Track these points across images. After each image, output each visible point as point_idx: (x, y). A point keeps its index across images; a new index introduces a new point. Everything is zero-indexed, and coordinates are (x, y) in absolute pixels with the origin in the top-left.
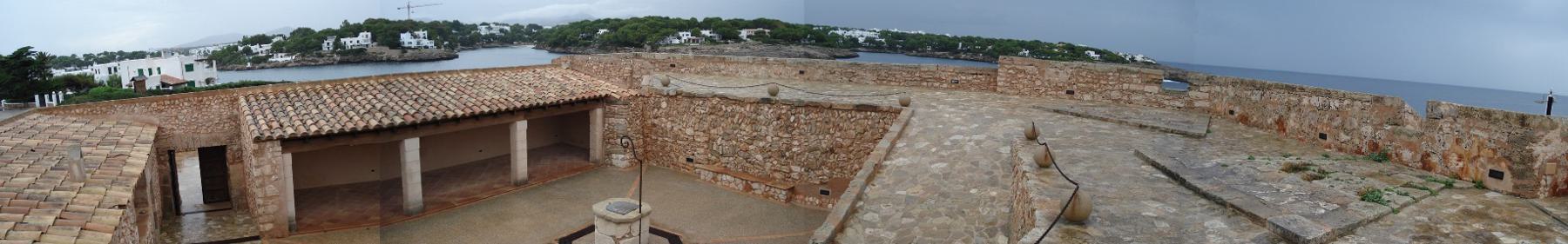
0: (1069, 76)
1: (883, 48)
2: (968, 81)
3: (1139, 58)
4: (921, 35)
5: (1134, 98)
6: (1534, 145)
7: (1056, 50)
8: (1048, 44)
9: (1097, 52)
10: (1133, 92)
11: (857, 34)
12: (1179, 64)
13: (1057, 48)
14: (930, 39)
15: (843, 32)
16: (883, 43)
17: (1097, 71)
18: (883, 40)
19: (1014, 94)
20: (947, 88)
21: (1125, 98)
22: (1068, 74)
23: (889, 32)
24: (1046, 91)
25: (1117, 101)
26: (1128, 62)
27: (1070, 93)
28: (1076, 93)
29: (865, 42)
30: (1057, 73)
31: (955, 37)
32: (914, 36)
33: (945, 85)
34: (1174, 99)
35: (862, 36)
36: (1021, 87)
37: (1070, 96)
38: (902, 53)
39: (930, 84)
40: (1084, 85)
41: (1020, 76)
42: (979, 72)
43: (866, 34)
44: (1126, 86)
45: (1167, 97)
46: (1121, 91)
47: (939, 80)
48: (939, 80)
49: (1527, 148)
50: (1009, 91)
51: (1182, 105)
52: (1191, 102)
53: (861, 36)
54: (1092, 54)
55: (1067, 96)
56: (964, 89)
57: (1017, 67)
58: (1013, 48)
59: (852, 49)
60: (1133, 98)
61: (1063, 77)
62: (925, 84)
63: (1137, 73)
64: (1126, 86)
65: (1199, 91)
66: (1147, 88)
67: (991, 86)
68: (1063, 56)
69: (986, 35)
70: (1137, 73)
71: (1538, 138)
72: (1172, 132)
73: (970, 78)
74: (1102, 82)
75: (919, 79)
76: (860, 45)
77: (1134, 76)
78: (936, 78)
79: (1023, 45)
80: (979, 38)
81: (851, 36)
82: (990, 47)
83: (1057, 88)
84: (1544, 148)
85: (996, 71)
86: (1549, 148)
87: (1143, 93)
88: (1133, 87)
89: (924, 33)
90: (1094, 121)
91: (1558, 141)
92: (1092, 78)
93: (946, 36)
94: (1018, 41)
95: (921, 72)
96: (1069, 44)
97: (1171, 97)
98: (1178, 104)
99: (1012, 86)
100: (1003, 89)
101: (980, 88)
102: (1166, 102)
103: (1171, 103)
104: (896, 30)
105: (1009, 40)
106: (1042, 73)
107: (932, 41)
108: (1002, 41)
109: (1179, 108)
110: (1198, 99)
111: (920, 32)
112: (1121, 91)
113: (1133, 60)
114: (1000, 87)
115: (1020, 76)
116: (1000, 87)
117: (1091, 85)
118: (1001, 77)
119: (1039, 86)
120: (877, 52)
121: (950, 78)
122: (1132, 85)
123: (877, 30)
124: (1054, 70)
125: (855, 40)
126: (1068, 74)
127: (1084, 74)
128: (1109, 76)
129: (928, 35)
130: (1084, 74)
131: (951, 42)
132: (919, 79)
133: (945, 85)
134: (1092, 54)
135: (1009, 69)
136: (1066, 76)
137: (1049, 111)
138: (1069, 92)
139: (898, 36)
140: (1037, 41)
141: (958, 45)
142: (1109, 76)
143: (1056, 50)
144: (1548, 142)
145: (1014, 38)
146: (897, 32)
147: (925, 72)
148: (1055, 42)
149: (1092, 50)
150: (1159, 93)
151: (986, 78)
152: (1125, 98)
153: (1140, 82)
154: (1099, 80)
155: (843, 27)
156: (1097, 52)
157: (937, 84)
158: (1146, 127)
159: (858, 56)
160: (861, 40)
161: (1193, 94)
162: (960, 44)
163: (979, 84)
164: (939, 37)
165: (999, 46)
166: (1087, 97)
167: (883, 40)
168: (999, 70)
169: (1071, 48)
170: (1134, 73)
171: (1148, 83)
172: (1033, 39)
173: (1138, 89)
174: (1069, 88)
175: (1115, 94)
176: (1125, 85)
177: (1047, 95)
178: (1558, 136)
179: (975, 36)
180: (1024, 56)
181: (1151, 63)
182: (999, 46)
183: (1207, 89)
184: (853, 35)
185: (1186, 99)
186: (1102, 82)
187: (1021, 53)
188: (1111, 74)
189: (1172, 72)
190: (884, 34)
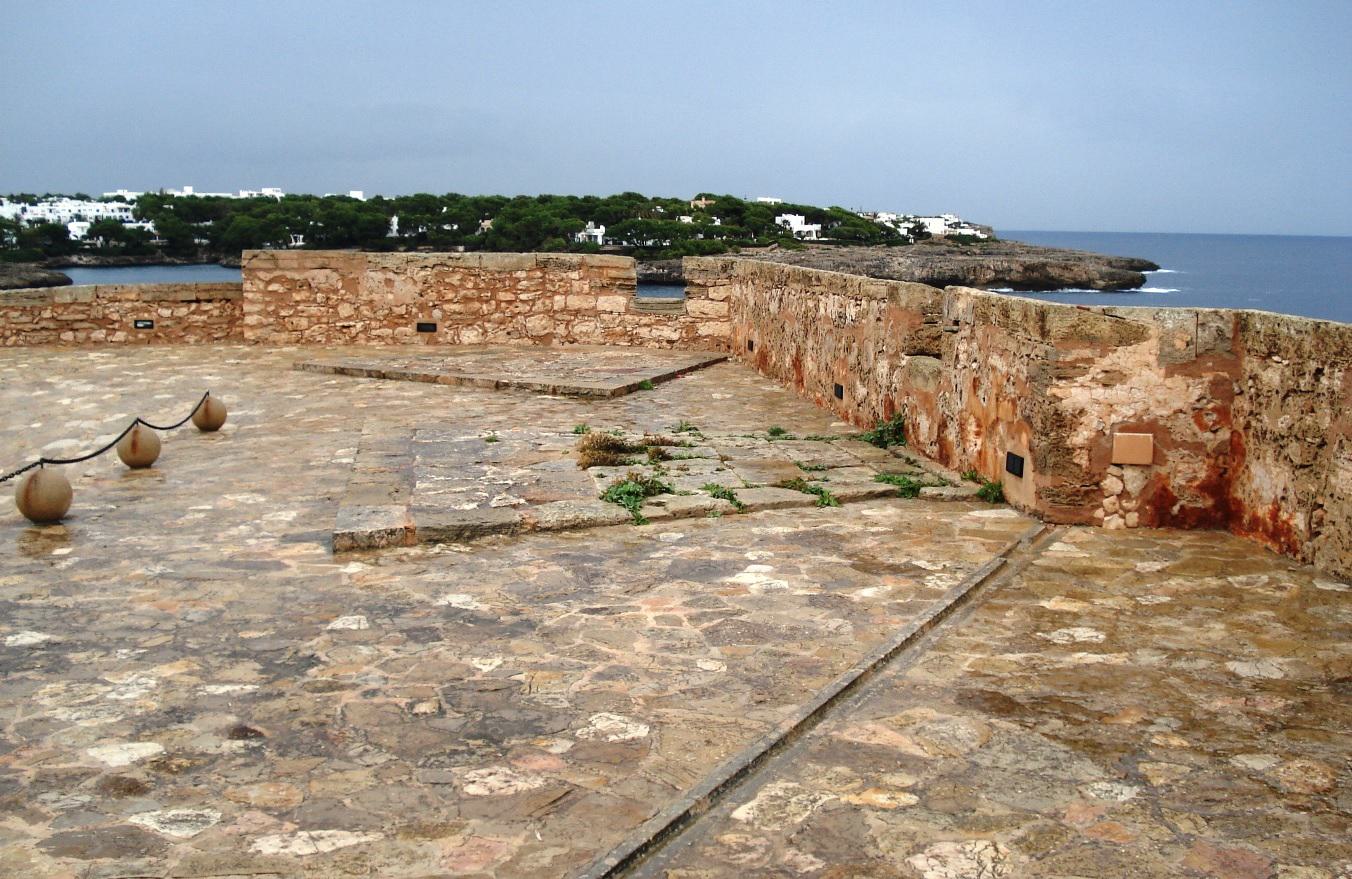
0: (420, 286)
1: (152, 250)
2: (179, 320)
3: (936, 227)
4: (272, 200)
5: (579, 328)
6: (1062, 383)
7: (687, 220)
8: (664, 203)
9: (812, 215)
10: (577, 312)
11: (61, 211)
12: (1024, 234)
13: (689, 213)
14: (299, 211)
15: (16, 208)
16: (149, 235)
17: (485, 270)
18: (149, 226)
19: (288, 343)
20: (125, 343)
21: (561, 330)
22: (415, 282)
23: (164, 198)
24: (366, 329)
25: (544, 340)
26: (904, 241)
27: (426, 328)
28: (442, 328)
29: (92, 233)
30: (389, 282)
31: (379, 199)
32: (247, 206)
33: (120, 336)
34: (658, 322)
35: (79, 218)
36: (304, 322)
37: (427, 335)
38: (214, 261)
39: (81, 335)
40: (456, 307)
41: (297, 297)
42: (203, 296)
43: (93, 210)
44: (559, 301)
45: (645, 320)
46: (550, 313)
47: (103, 322)
48: (103, 322)
49: (1049, 392)
50: (275, 336)
51: (675, 336)
52: (691, 327)
53: (74, 216)
54: (797, 223)
55: (418, 338)
56: (170, 342)
57: (290, 275)
58: (557, 221)
59: (50, 260)
60: (577, 330)
61: (405, 290)
62: (68, 336)
63: (580, 266)
64: (559, 301)
65: (707, 298)
66: (605, 302)
67: (230, 329)
68: (709, 235)
69: (474, 188)
70: (580, 266)
71: (1073, 365)
72: (554, 392)
73: (183, 311)
74: (502, 296)
75: (52, 325)
76: (76, 247)
77: (574, 275)
78: (94, 320)
79: (587, 209)
80: (453, 199)
81: (42, 221)
82: (487, 224)
83: (394, 320)
84: (1099, 392)
85: (239, 288)
86: (1118, 392)
87: (596, 313)
88: (574, 302)
89: (279, 195)
90: (399, 384)
91: (1155, 375)
92: (476, 287)
93: (350, 200)
94: (572, 198)
95: (55, 306)
96: (728, 199)
97: (653, 319)
98: (668, 333)
99: (281, 325)
100: (259, 332)
101: (208, 334)
102: (644, 332)
103: (655, 333)
104: (188, 191)
105: (544, 200)
106: (352, 285)
107: (307, 216)
108: (523, 201)
109: (669, 342)
110: (705, 318)
111: (267, 192)
112: (550, 313)
113: (919, 232)
114: (252, 327)
115: (297, 297)
116: (252, 327)
117: (477, 305)
118: (252, 302)
119: (348, 318)
120: (130, 265)
121: (130, 319)
122: (570, 297)
123: (130, 196)
124: (380, 276)
125: (58, 231)
126: (415, 282)
127: (455, 279)
128: (519, 280)
129: (291, 198)
130: (455, 279)
131: (366, 217)
132: (52, 325)
133: (120, 336)
134: (797, 223)
135: (269, 282)
136: (410, 286)
137: (324, 371)
138: (423, 328)
139: (194, 209)
140: (629, 196)
141: (387, 225)
142: (519, 280)
143: (687, 220)
144: (1111, 379)
145: (561, 190)
146: (193, 197)
147: (66, 306)
148: (687, 195)
149: (795, 210)
150: (627, 311)
151: (222, 308)
152: (561, 330)
153: (586, 288)
154: (495, 291)
155: (17, 193)
156: (812, 215)
157: (100, 334)
158: (507, 385)
159: (68, 282)
160: (77, 230)
161: (693, 305)
162: (395, 220)
163: (205, 325)
164: (327, 203)
165: (515, 218)
166: (469, 336)
167: (149, 226)
168: (247, 286)
169: (731, 209)
170: (571, 267)
171: (604, 289)
172: (619, 191)
173: (585, 305)
174: (422, 318)
175: (537, 324)
176: (557, 298)
177: (369, 339)
178: (1152, 359)
179: (439, 191)
180: (590, 247)
181: (974, 238)
182: (515, 218)
183: (722, 292)
184: (51, 218)
185: (682, 319)
186: (502, 296)
187: (581, 236)
188: (521, 274)
189: (1029, 260)
190: (149, 206)
